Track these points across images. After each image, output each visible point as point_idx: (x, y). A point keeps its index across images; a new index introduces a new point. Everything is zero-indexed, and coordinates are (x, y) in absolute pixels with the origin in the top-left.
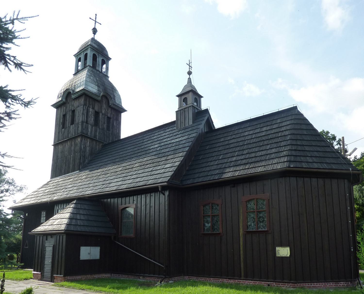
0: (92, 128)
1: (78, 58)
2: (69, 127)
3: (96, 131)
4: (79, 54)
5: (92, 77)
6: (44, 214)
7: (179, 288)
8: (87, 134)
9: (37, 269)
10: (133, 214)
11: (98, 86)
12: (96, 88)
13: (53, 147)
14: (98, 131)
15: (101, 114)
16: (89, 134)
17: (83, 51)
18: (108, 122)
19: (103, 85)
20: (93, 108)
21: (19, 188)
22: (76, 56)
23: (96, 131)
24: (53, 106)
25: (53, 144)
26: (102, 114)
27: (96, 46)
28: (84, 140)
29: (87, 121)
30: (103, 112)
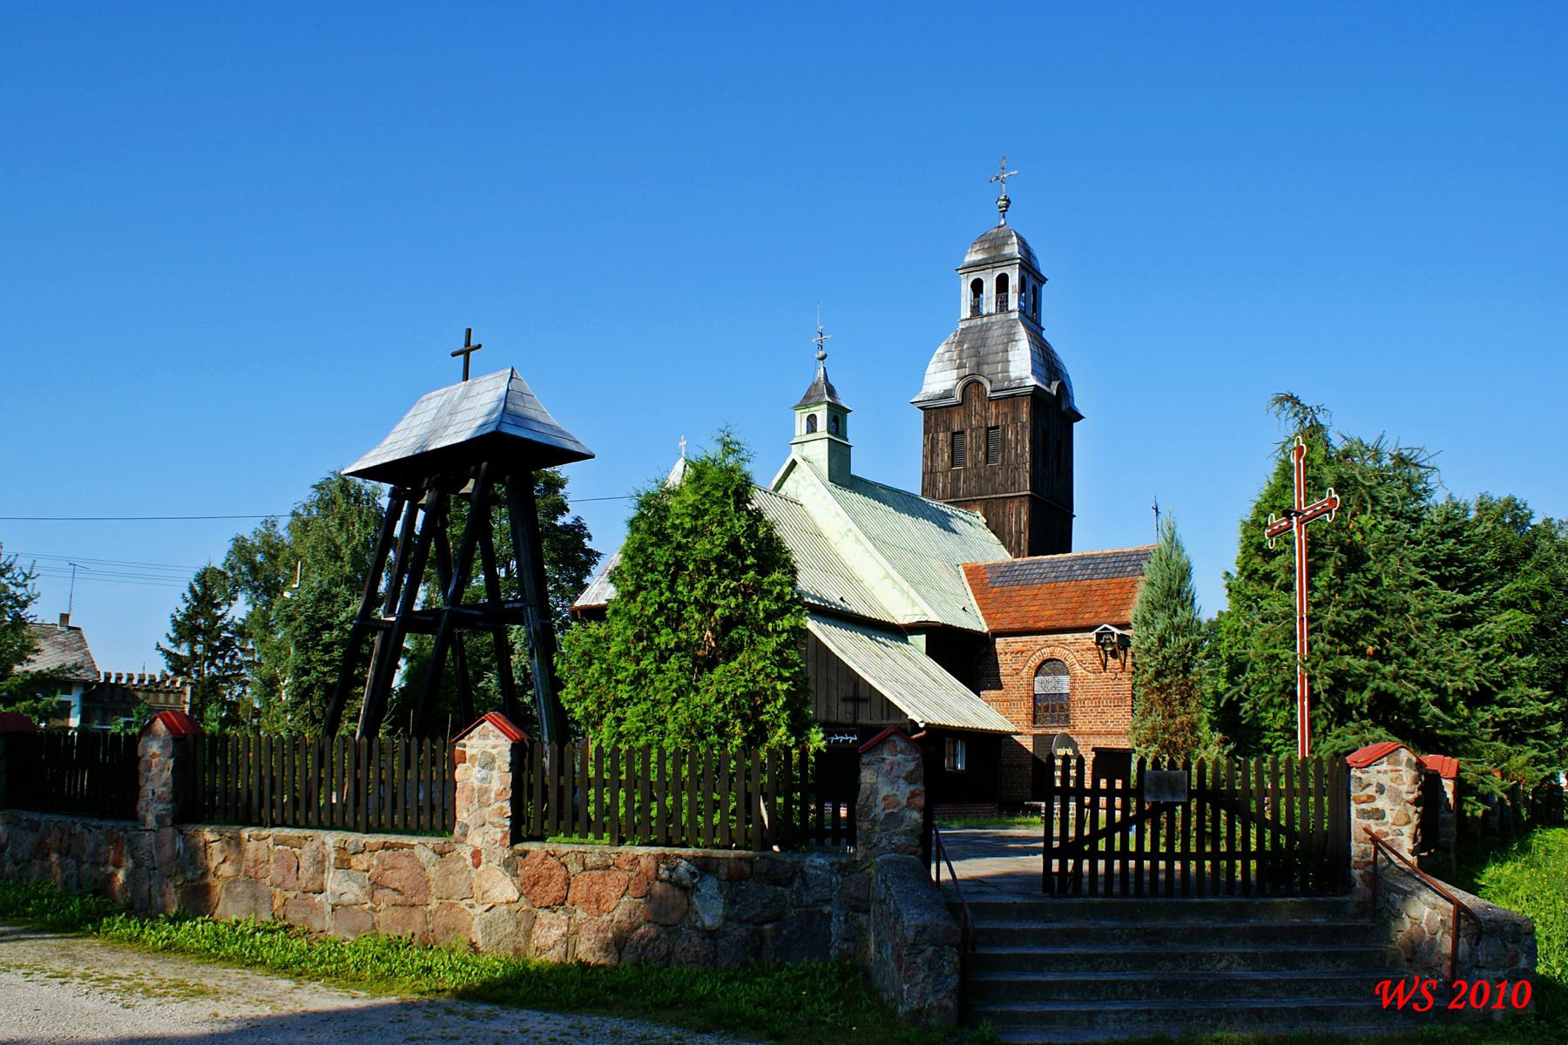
3: (956, 478)
26: (972, 430)
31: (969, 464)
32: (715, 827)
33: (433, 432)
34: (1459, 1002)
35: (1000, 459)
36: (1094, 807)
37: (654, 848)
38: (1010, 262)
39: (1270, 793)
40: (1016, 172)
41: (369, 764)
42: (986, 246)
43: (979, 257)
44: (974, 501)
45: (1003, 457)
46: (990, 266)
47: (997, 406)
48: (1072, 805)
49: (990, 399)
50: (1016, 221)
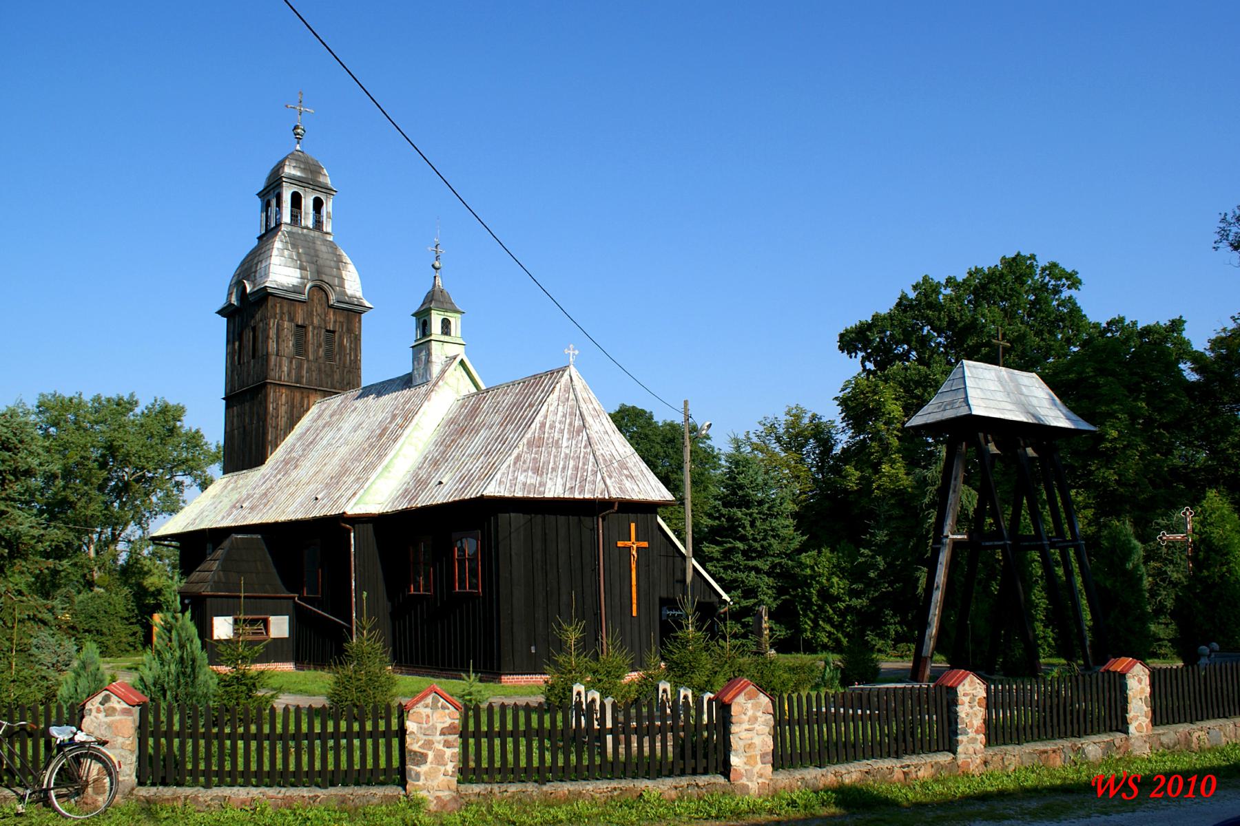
0: (291, 362)
1: (266, 200)
2: (249, 362)
3: (300, 367)
4: (265, 192)
5: (286, 252)
6: (209, 546)
7: (443, 680)
8: (280, 379)
9: (1185, 717)
10: (1139, 328)
11: (302, 268)
12: (297, 273)
13: (224, 402)
14: (305, 366)
15: (311, 328)
16: (284, 376)
17: (273, 188)
18: (329, 342)
19: (313, 263)
20: (291, 320)
21: (437, 265)
22: (261, 195)
23: (300, 367)
24: (220, 312)
25: (224, 396)
26: (314, 328)
27: (299, 174)
28: (274, 392)
29: (278, 350)
30: (315, 321)
31: (311, 357)
32: (648, 735)
33: (339, 412)
34: (1159, 792)
35: (337, 360)
36: (337, 748)
37: (380, 748)
38: (328, 191)
39: (3, 772)
40: (312, 111)
41: (1039, 721)
42: (302, 166)
43: (298, 173)
44: (316, 390)
45: (340, 359)
46: (311, 187)
47: (334, 314)
48: (535, 744)
49: (331, 307)
50: (311, 148)
